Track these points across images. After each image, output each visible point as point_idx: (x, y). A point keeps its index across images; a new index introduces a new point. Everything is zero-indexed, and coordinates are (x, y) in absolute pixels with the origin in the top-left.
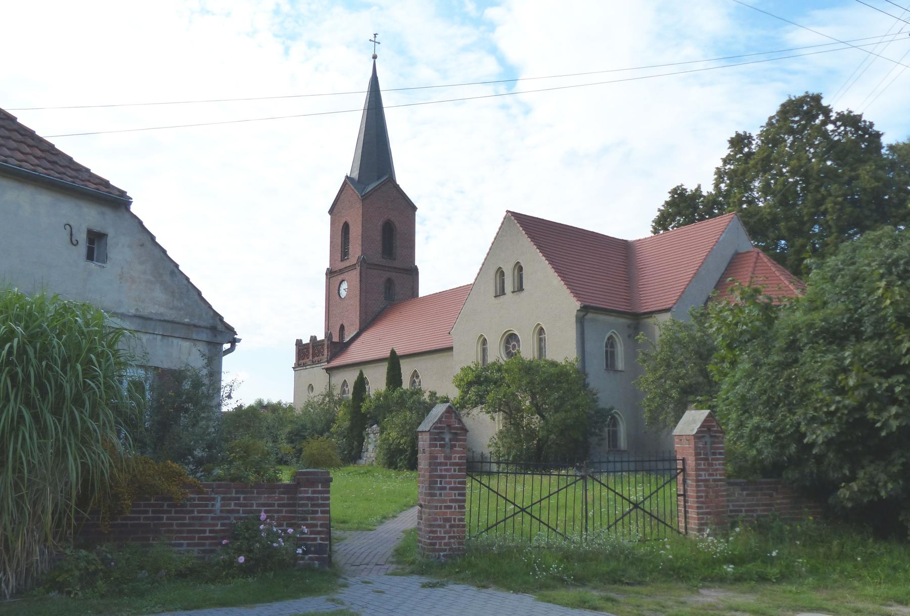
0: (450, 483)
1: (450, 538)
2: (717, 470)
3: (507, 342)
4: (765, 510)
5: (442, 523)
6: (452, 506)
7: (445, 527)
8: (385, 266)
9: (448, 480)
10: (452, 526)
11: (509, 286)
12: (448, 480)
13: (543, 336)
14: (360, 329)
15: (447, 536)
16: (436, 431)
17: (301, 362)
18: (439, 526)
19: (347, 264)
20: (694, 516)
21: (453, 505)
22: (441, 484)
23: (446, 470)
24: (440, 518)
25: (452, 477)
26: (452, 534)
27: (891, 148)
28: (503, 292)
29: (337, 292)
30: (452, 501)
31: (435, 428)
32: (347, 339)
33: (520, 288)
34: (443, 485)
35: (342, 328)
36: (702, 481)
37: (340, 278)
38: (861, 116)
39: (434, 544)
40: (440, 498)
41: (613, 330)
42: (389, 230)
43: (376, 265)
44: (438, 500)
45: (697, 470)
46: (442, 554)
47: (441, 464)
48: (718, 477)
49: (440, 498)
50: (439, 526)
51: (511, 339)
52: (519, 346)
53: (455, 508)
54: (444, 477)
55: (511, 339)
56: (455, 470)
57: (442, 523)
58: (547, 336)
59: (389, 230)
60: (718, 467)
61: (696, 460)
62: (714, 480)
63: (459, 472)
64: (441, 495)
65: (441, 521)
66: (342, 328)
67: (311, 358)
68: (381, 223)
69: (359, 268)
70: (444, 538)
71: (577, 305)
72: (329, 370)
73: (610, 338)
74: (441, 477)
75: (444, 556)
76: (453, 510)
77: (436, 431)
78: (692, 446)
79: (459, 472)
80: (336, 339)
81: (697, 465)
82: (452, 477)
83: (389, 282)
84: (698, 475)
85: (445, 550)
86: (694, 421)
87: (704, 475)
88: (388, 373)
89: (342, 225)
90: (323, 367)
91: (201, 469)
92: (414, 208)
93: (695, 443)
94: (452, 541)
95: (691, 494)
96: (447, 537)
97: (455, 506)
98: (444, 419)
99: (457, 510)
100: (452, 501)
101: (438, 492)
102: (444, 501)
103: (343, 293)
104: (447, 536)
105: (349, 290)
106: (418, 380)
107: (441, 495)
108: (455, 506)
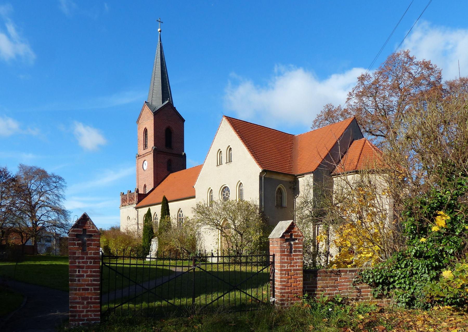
0: (86, 272)
1: (87, 311)
2: (296, 262)
3: (223, 191)
4: (331, 290)
5: (81, 300)
6: (298, 267)
7: (83, 303)
8: (164, 152)
9: (85, 269)
10: (88, 303)
11: (224, 160)
12: (85, 269)
13: (242, 188)
14: (154, 187)
15: (85, 310)
16: (74, 233)
17: (124, 204)
18: (78, 303)
19: (147, 151)
20: (278, 294)
21: (89, 288)
22: (79, 272)
23: (83, 262)
24: (79, 298)
25: (88, 267)
26: (89, 309)
27: (446, 83)
28: (221, 164)
29: (142, 167)
30: (88, 285)
31: (73, 231)
32: (147, 192)
33: (230, 161)
34: (81, 273)
35: (145, 186)
36: (285, 270)
37: (143, 159)
38: (430, 62)
39: (75, 316)
40: (79, 283)
41: (281, 184)
42: (169, 132)
43: (162, 152)
44: (77, 284)
45: (281, 262)
46: (81, 323)
47: (78, 258)
48: (297, 268)
49: (79, 283)
50: (78, 303)
51: (225, 190)
52: (229, 194)
53: (91, 290)
54: (82, 267)
55: (225, 190)
56: (91, 263)
57: (81, 300)
58: (244, 187)
59: (169, 132)
60: (298, 260)
61: (281, 255)
62: (294, 270)
63: (94, 264)
64: (79, 280)
65: (79, 299)
66: (145, 186)
67: (128, 202)
68: (164, 129)
69: (153, 153)
70: (82, 312)
71: (260, 170)
72: (137, 208)
73: (279, 189)
74: (79, 267)
75: (82, 324)
76: (89, 291)
77: (74, 233)
78: (279, 245)
79: (94, 264)
80: (141, 192)
81: (282, 259)
82: (88, 267)
83: (169, 161)
84: (281, 266)
85: (83, 320)
86: (282, 229)
87: (286, 266)
88: (162, 209)
89: (143, 130)
90: (134, 207)
91: (179, 257)
92: (183, 121)
93: (281, 243)
94: (89, 313)
95: (277, 279)
96: (85, 311)
97: (91, 289)
98: (80, 225)
99: (93, 291)
100: (88, 285)
101: (77, 279)
102: (82, 285)
103: (145, 167)
104: (85, 310)
105: (148, 166)
106: (182, 214)
107: (79, 280)
108: (91, 289)
